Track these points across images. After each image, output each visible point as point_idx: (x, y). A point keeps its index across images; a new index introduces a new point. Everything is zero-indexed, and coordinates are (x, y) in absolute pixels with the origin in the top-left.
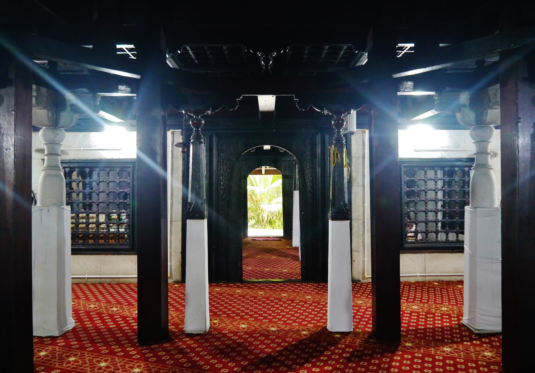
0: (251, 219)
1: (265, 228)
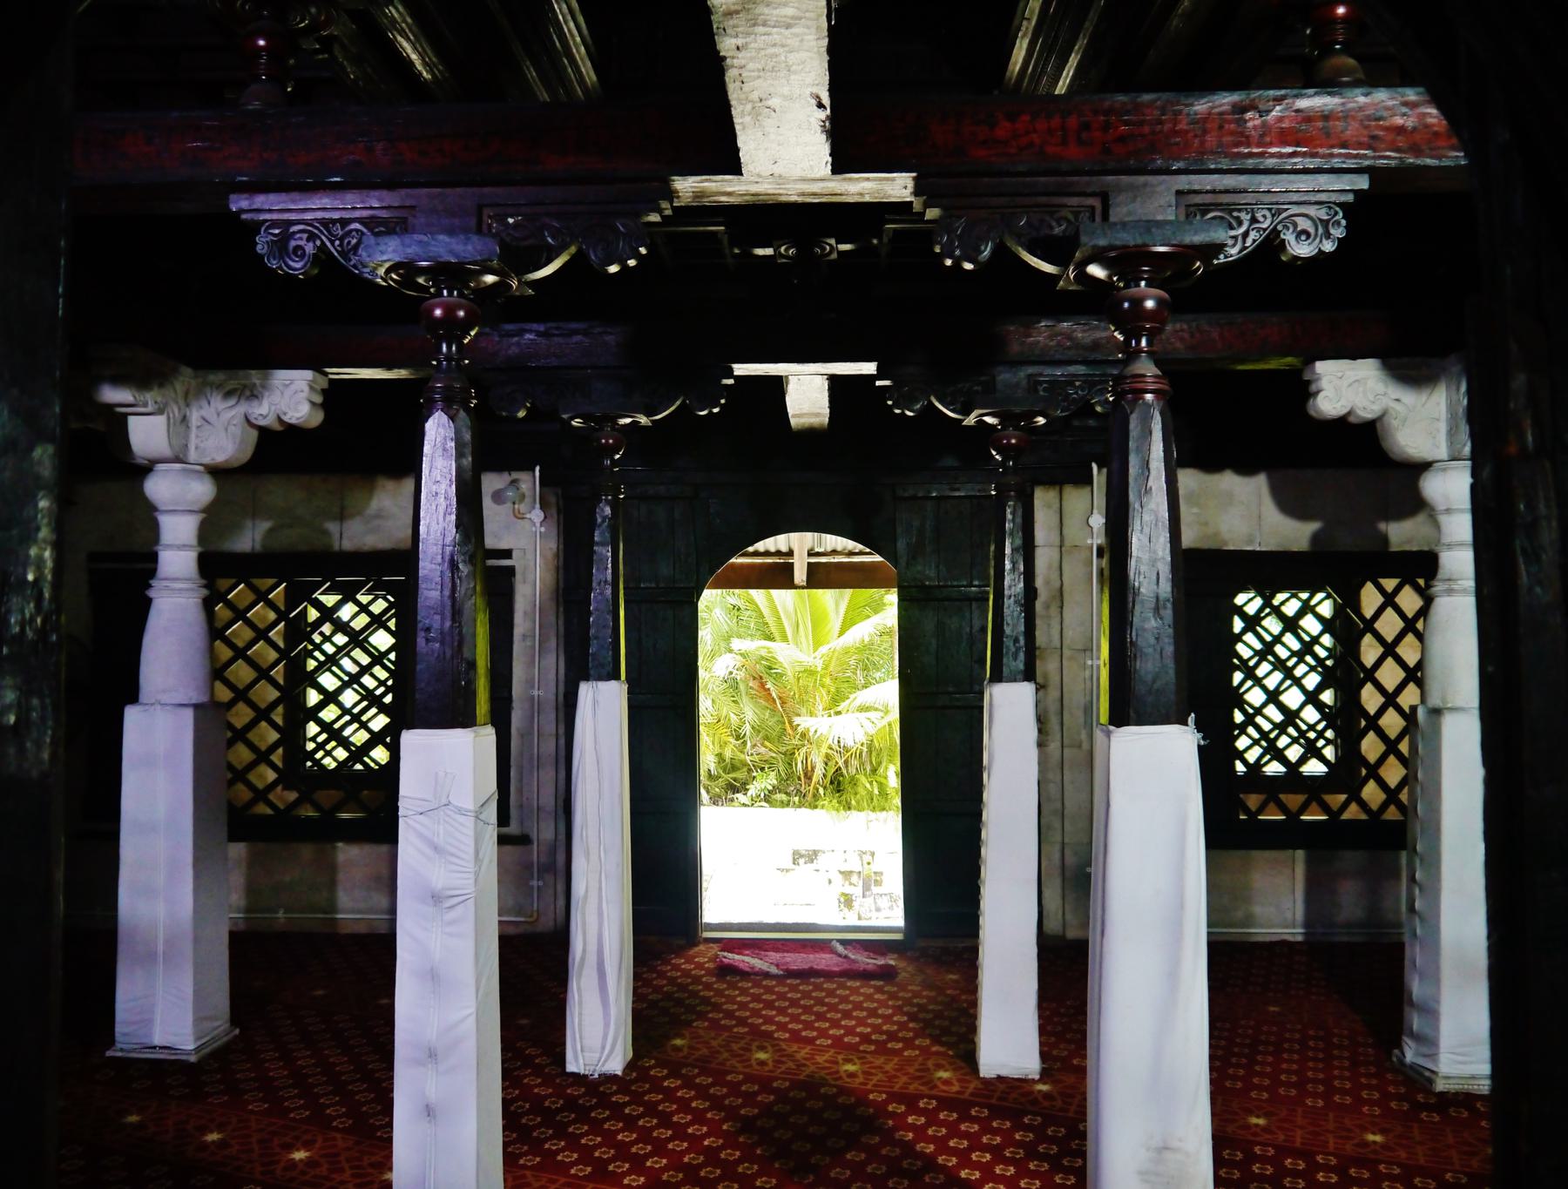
0: (762, 769)
1: (816, 807)
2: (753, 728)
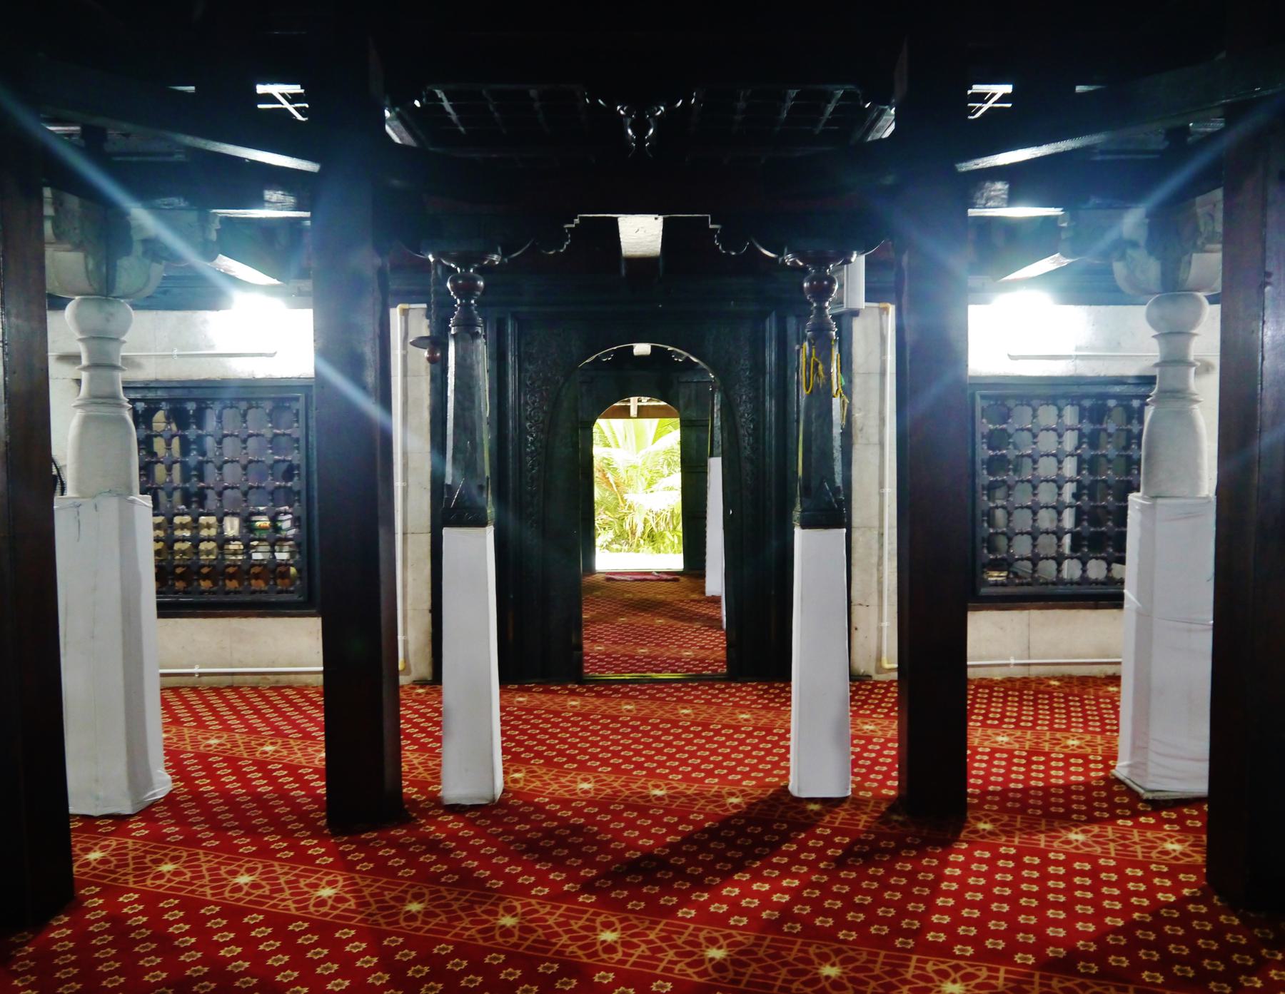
1: (638, 552)
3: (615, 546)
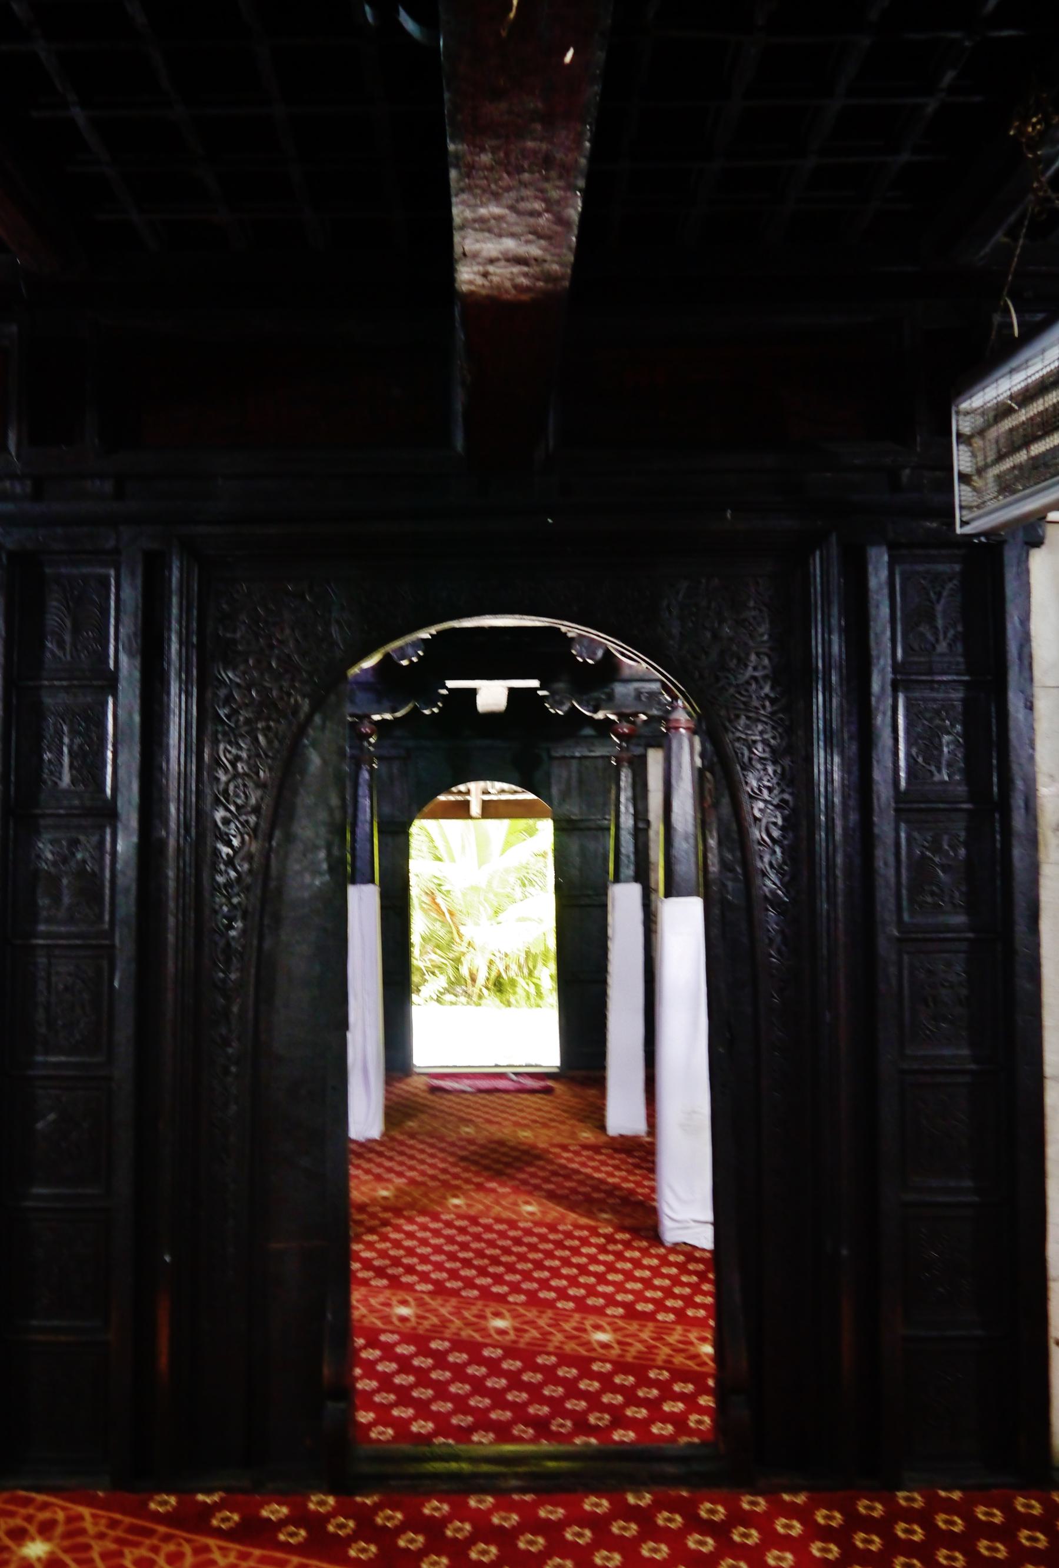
0: (433, 973)
2: (423, 938)
3: (448, 997)
